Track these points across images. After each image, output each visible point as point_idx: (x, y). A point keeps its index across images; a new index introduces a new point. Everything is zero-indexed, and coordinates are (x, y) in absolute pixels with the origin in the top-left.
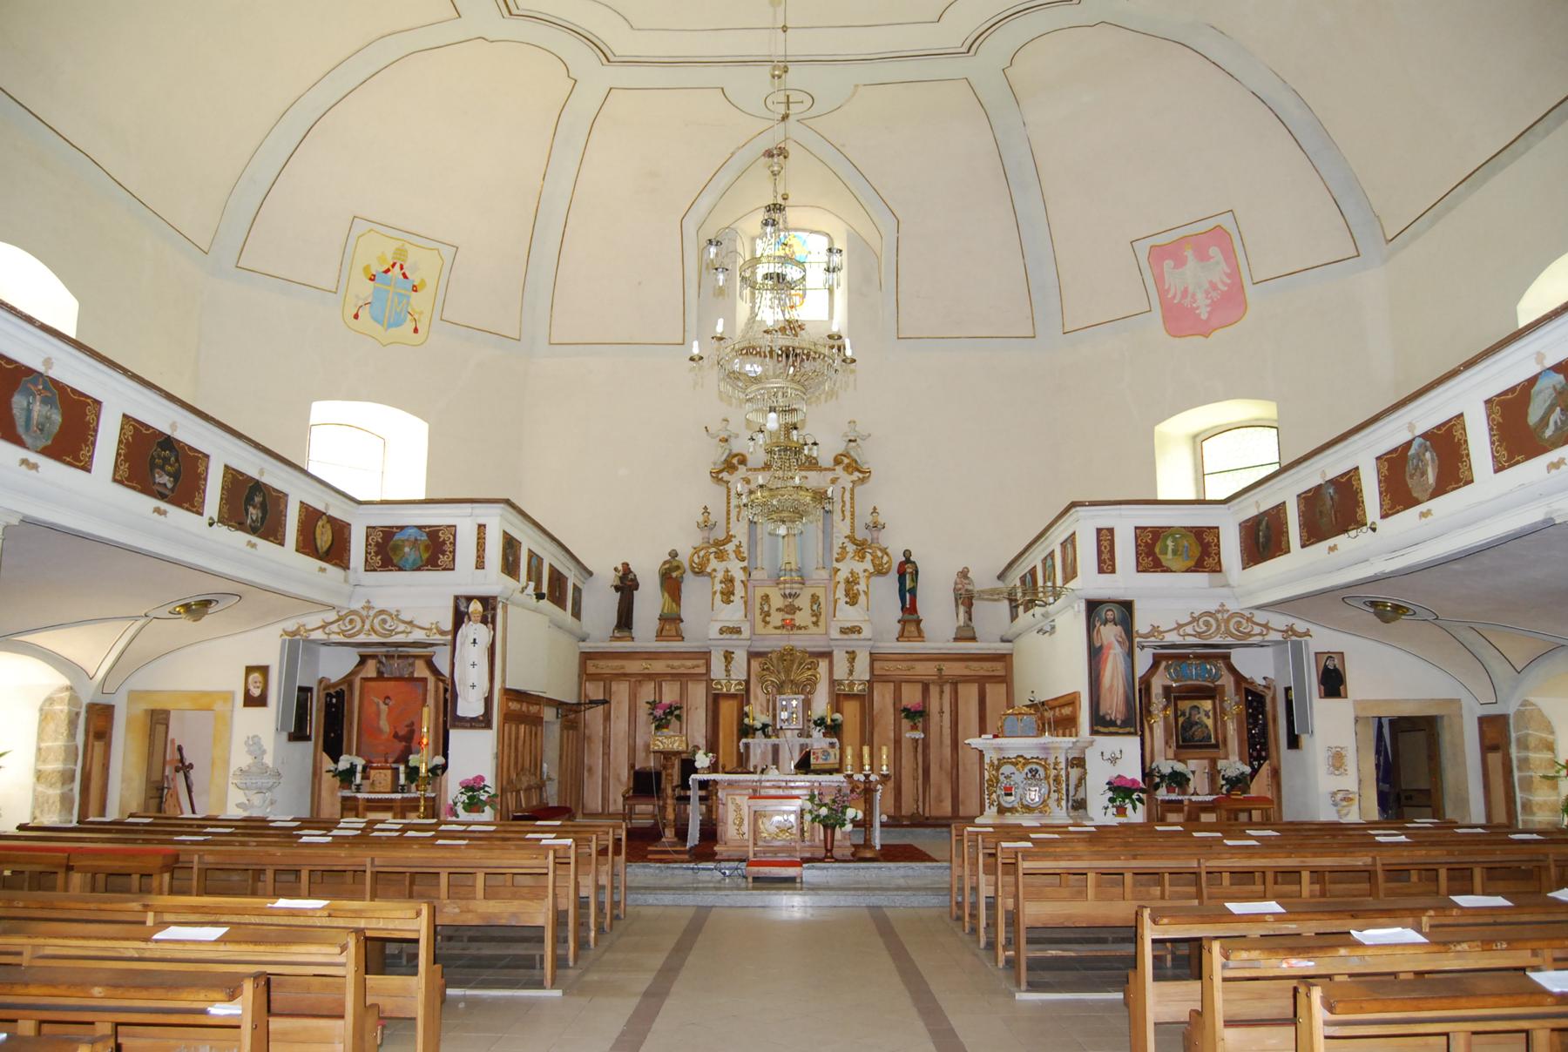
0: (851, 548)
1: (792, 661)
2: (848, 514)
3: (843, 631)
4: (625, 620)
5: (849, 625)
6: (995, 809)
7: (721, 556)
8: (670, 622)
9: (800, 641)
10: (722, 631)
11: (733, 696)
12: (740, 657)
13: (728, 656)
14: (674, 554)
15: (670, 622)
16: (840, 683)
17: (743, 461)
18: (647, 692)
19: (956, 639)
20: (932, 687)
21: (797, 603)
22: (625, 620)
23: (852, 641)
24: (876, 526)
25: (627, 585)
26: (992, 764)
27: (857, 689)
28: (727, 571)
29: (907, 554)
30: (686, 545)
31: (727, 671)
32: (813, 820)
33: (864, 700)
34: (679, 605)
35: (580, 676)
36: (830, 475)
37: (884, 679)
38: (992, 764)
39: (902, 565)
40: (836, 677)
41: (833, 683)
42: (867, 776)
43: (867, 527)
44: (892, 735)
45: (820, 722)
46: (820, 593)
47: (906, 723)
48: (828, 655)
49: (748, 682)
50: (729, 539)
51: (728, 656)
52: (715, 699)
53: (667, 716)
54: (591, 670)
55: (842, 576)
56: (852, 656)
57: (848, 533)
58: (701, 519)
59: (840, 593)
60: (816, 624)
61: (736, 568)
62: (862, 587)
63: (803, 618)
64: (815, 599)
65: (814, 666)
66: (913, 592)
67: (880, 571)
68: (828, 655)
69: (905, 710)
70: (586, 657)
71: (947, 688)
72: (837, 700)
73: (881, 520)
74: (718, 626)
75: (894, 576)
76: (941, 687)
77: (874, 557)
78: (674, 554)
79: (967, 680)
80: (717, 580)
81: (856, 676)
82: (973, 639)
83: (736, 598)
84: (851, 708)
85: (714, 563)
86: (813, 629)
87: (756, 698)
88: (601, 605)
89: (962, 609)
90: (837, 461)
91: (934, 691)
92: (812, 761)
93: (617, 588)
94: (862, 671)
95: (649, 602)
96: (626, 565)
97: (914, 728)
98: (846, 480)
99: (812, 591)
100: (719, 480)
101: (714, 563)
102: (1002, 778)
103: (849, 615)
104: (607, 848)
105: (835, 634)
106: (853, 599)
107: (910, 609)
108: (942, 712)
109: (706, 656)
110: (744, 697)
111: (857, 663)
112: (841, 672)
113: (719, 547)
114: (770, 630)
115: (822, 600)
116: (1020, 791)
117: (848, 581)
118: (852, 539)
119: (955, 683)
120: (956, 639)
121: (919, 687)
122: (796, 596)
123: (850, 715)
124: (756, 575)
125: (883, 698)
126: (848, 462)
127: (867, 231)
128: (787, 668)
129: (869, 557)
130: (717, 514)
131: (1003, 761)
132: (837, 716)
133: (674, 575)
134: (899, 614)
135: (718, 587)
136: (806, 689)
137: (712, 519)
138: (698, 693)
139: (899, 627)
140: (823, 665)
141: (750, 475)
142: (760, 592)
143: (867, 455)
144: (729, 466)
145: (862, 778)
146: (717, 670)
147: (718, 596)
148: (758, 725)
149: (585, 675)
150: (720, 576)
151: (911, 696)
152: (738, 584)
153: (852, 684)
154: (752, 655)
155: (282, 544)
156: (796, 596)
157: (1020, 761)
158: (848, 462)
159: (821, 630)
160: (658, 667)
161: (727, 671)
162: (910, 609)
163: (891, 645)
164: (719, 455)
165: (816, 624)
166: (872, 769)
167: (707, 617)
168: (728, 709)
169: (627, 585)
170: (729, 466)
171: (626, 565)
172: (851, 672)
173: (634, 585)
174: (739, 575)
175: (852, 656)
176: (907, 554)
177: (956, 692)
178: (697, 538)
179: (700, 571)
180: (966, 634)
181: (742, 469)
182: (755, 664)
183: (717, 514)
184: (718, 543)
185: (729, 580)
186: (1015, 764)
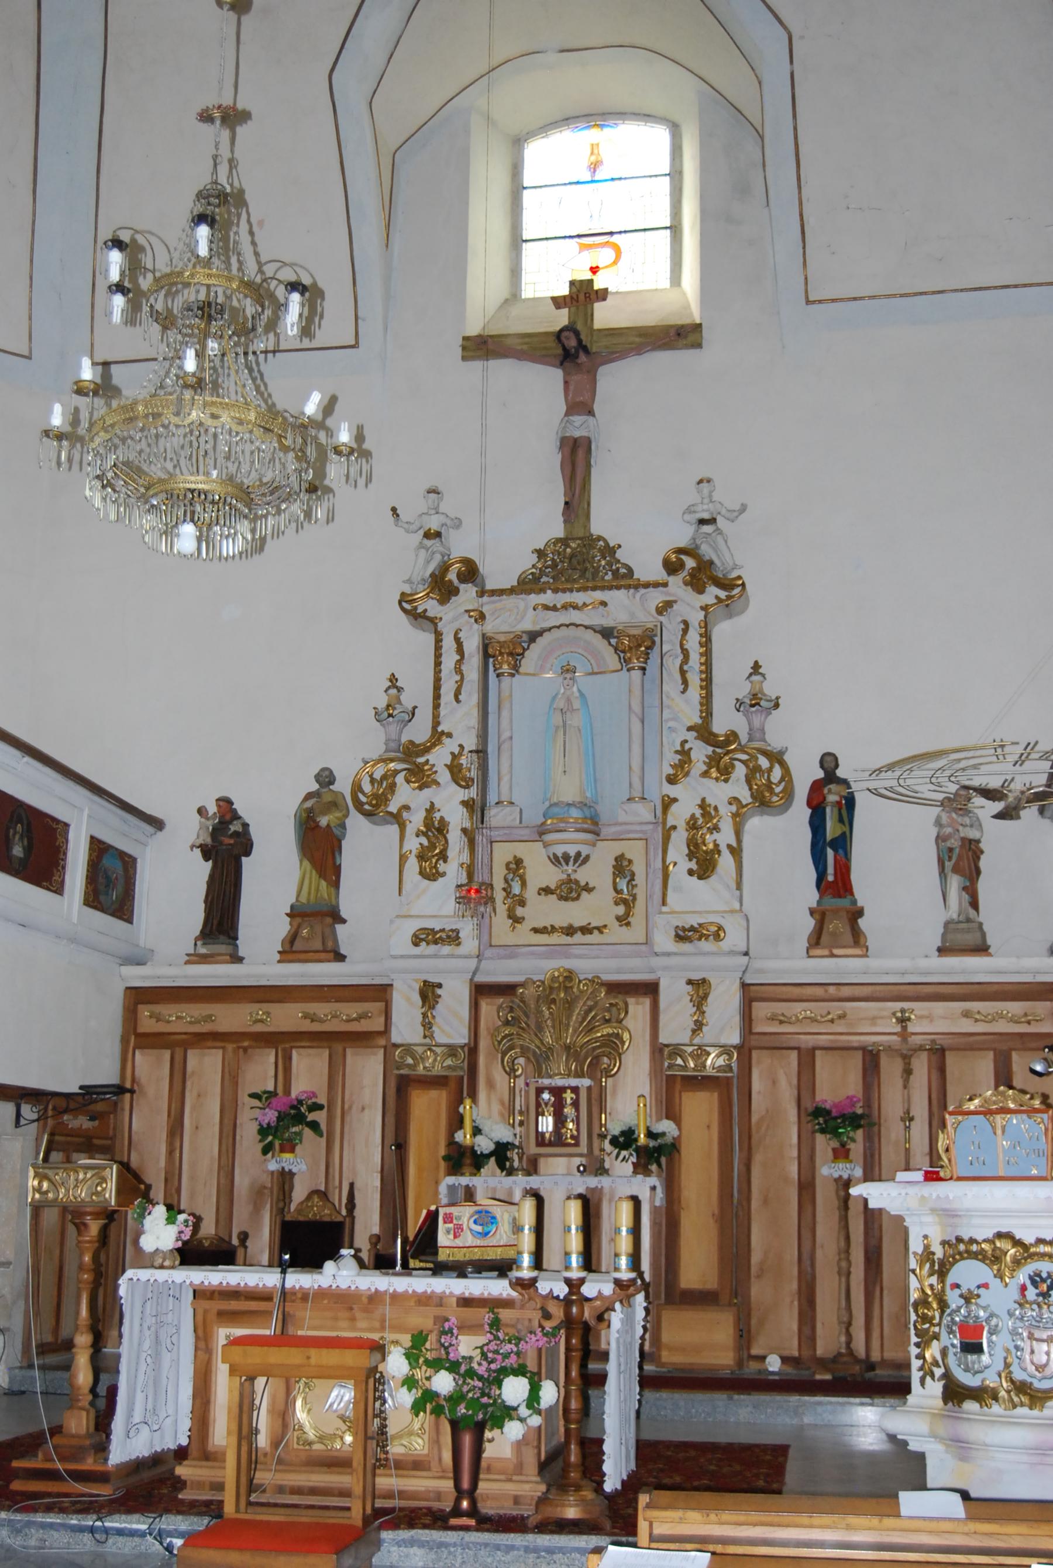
0: (700, 752)
1: (570, 1004)
2: (695, 679)
3: (683, 935)
4: (221, 920)
5: (694, 921)
6: (935, 1388)
7: (421, 777)
8: (315, 924)
9: (592, 963)
10: (416, 941)
11: (437, 1082)
12: (455, 999)
13: (429, 993)
14: (326, 778)
15: (315, 924)
16: (676, 1050)
17: (470, 572)
18: (261, 1071)
19: (942, 951)
20: (884, 1061)
21: (583, 875)
22: (221, 920)
23: (700, 959)
24: (756, 702)
25: (227, 845)
26: (927, 1255)
27: (713, 1061)
28: (431, 809)
29: (829, 762)
30: (353, 751)
31: (427, 1025)
32: (417, 1407)
33: (731, 1090)
34: (336, 884)
35: (125, 1041)
36: (656, 597)
37: (777, 1046)
38: (927, 1255)
39: (817, 787)
40: (663, 1039)
41: (658, 1051)
42: (574, 1285)
43: (739, 704)
44: (793, 1170)
45: (625, 1140)
46: (634, 851)
47: (823, 1144)
48: (650, 989)
49: (473, 1050)
50: (438, 737)
51: (429, 993)
52: (401, 1087)
53: (290, 1121)
54: (147, 1024)
55: (679, 815)
56: (700, 989)
57: (696, 720)
58: (382, 702)
59: (678, 850)
60: (624, 920)
61: (450, 801)
62: (726, 836)
63: (597, 907)
64: (621, 867)
65: (616, 1017)
66: (842, 844)
67: (765, 799)
68: (650, 989)
69: (818, 1112)
70: (138, 997)
71: (921, 1065)
72: (673, 1085)
73: (770, 689)
74: (412, 927)
75: (800, 812)
76: (907, 1058)
77: (753, 771)
78: (326, 778)
79: (970, 1044)
80: (410, 830)
81: (707, 1035)
82: (982, 949)
83: (453, 870)
84: (700, 1109)
85: (405, 793)
86: (616, 933)
87: (491, 1085)
88: (172, 883)
89: (955, 882)
90: (672, 567)
91: (890, 1069)
92: (443, 1238)
93: (207, 853)
94: (724, 1024)
95: (273, 880)
96: (225, 803)
97: (841, 1153)
98: (690, 605)
99: (617, 848)
100: (417, 616)
101: (405, 793)
102: (954, 1299)
103: (695, 898)
104: (52, 1435)
105: (664, 940)
106: (704, 865)
107: (835, 883)
108: (908, 1118)
109: (380, 993)
110: (462, 1085)
111: (712, 1006)
112: (675, 1028)
113: (412, 761)
114: (524, 935)
115: (639, 868)
116: (1003, 1340)
117: (692, 825)
118: (704, 731)
119: (938, 1054)
120: (942, 951)
121: (856, 1061)
122: (581, 860)
123: (698, 1123)
124: (496, 817)
125: (773, 1088)
126: (696, 568)
127: (734, 80)
128: (556, 1024)
129: (740, 770)
130: (417, 692)
131: (960, 1249)
132: (666, 1126)
133: (323, 821)
134: (812, 897)
135: (413, 844)
136: (600, 1058)
137: (407, 700)
138: (367, 1074)
139: (810, 923)
140: (638, 1009)
141: (488, 605)
142: (503, 854)
143: (736, 551)
144: (442, 587)
145: (561, 1290)
146: (405, 1027)
147: (412, 865)
148: (484, 1145)
149: (136, 1038)
150: (416, 820)
151: (837, 1084)
152: (455, 837)
153: (701, 1053)
154: (481, 991)
155: (59, 890)
156: (581, 860)
157: (1001, 1251)
158: (696, 568)
159: (636, 932)
160: (286, 1017)
161: (427, 1025)
162: (835, 883)
163: (792, 963)
164: (415, 565)
165: (624, 920)
166: (538, 1263)
167: (391, 911)
168: (426, 1109)
169: (227, 845)
170: (442, 587)
171: (225, 803)
172: (698, 1027)
173: (244, 844)
174: (456, 817)
175: (700, 989)
176: (829, 762)
177: (942, 1070)
178: (374, 741)
179: (375, 806)
180: (965, 938)
181: (468, 593)
182: (488, 1008)
183: (417, 692)
184: (411, 752)
185: (435, 829)
186: (995, 1259)
